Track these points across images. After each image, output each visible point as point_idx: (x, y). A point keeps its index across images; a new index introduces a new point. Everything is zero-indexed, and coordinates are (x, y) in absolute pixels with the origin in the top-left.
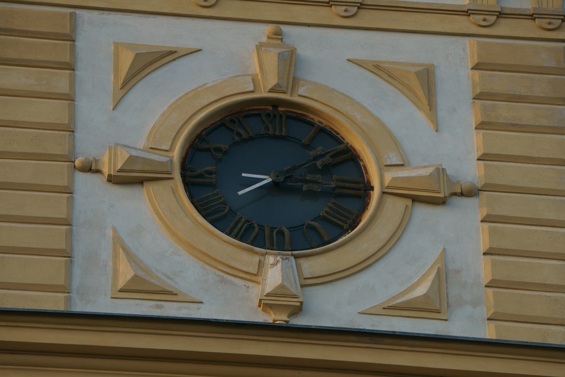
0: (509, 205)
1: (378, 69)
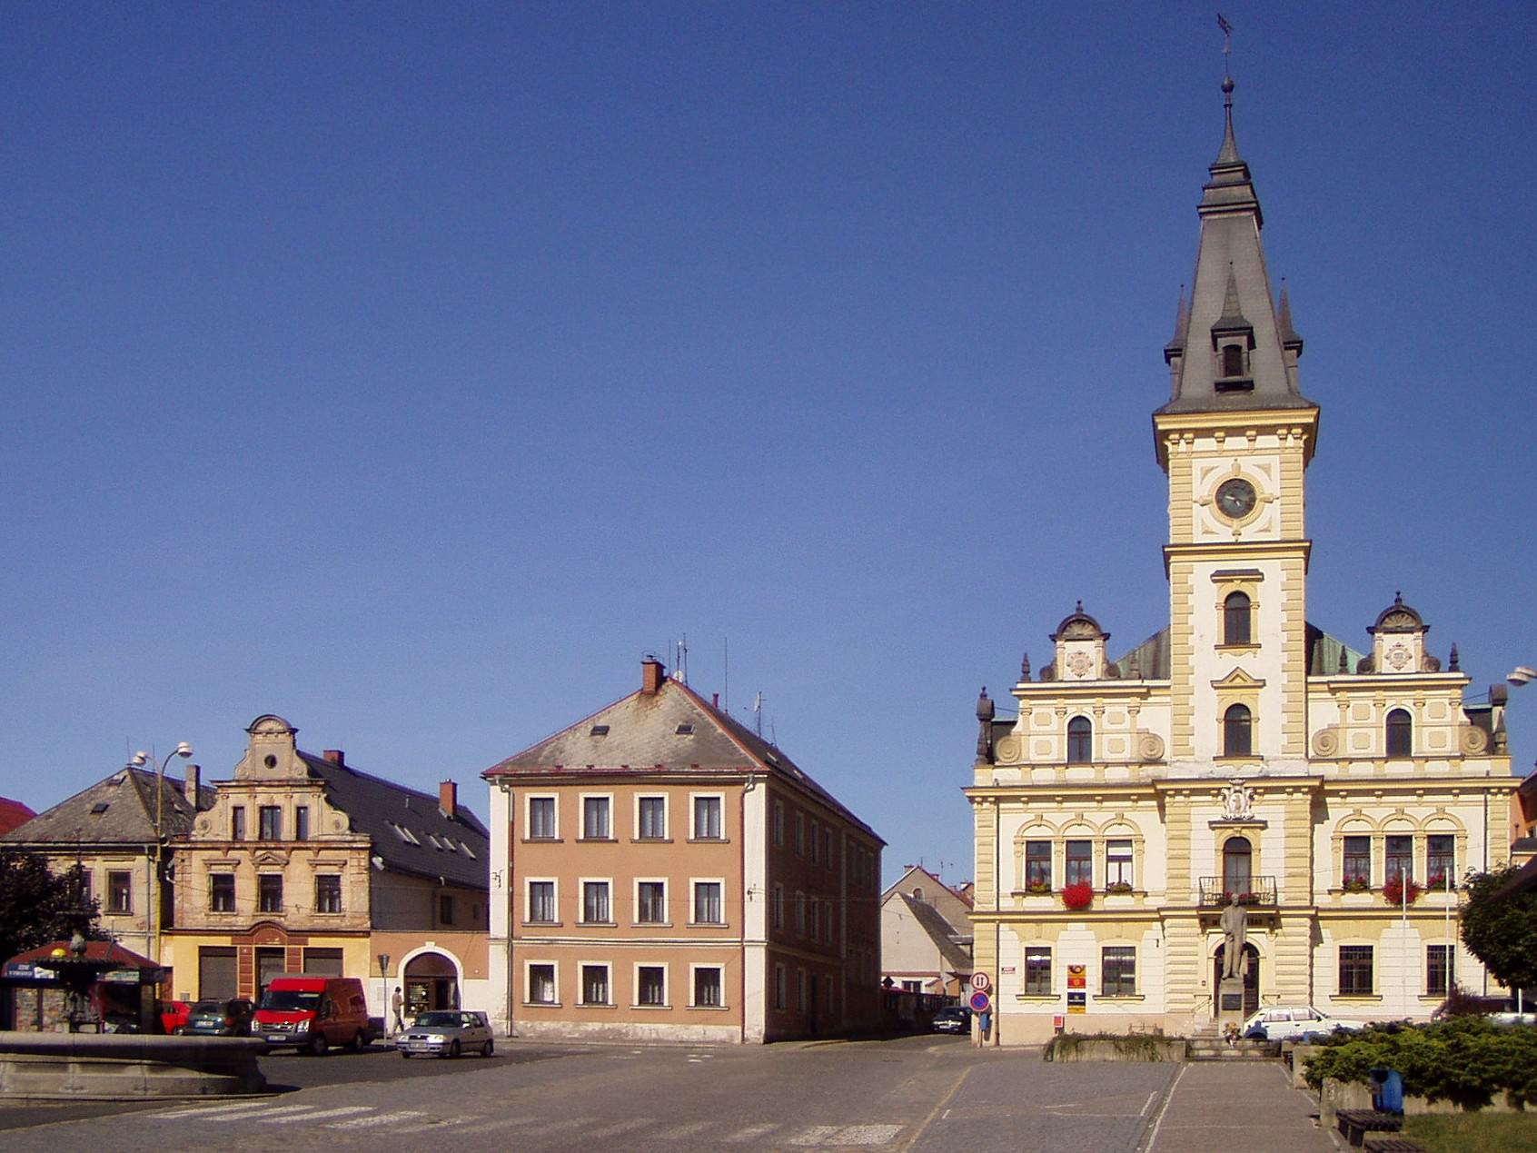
0: (1286, 500)
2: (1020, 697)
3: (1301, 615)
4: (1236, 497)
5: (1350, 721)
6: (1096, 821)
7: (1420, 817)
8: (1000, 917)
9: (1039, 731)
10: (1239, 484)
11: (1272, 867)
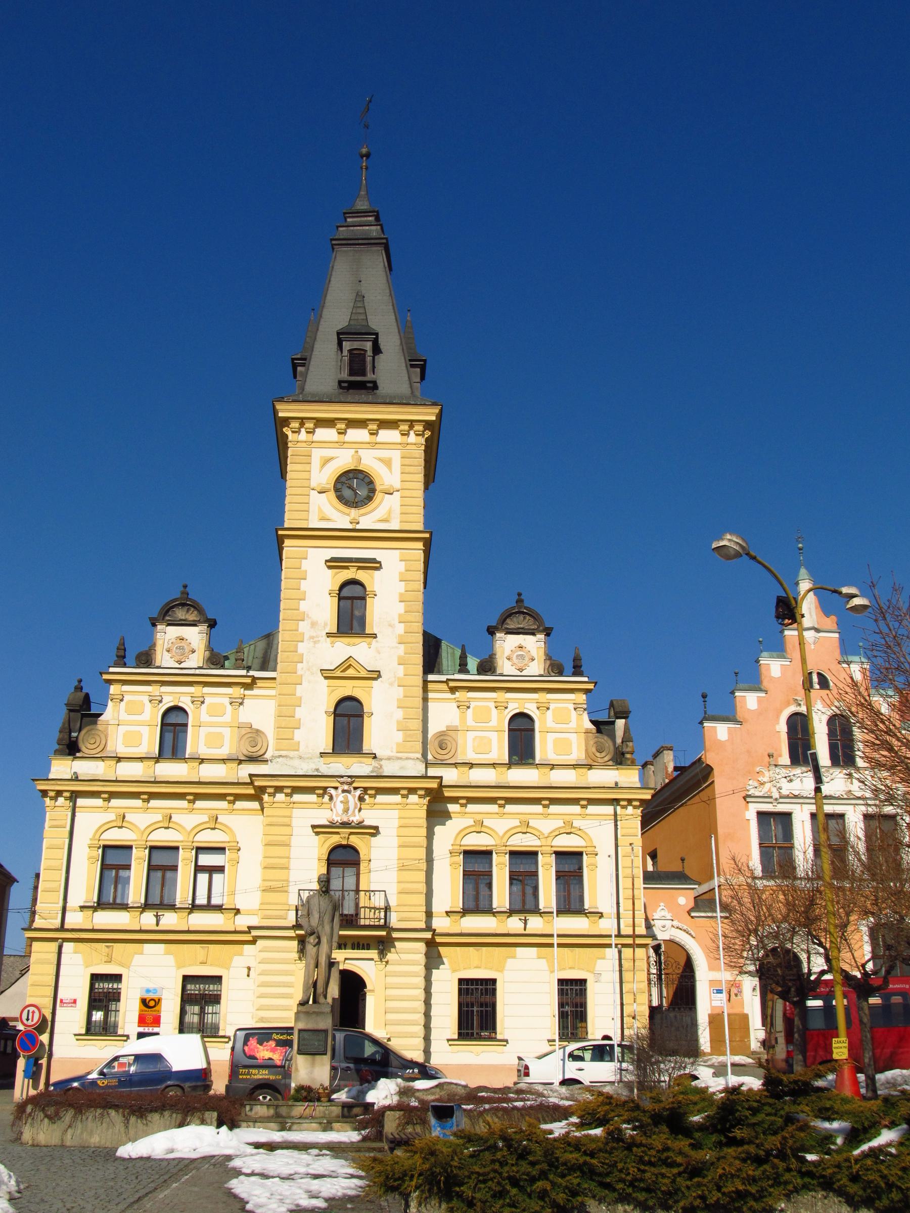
0: (407, 493)
1: (380, 460)
2: (110, 682)
3: (418, 628)
4: (354, 487)
5: (470, 722)
6: (186, 824)
7: (546, 831)
8: (62, 934)
9: (129, 718)
10: (355, 474)
11: (384, 876)
